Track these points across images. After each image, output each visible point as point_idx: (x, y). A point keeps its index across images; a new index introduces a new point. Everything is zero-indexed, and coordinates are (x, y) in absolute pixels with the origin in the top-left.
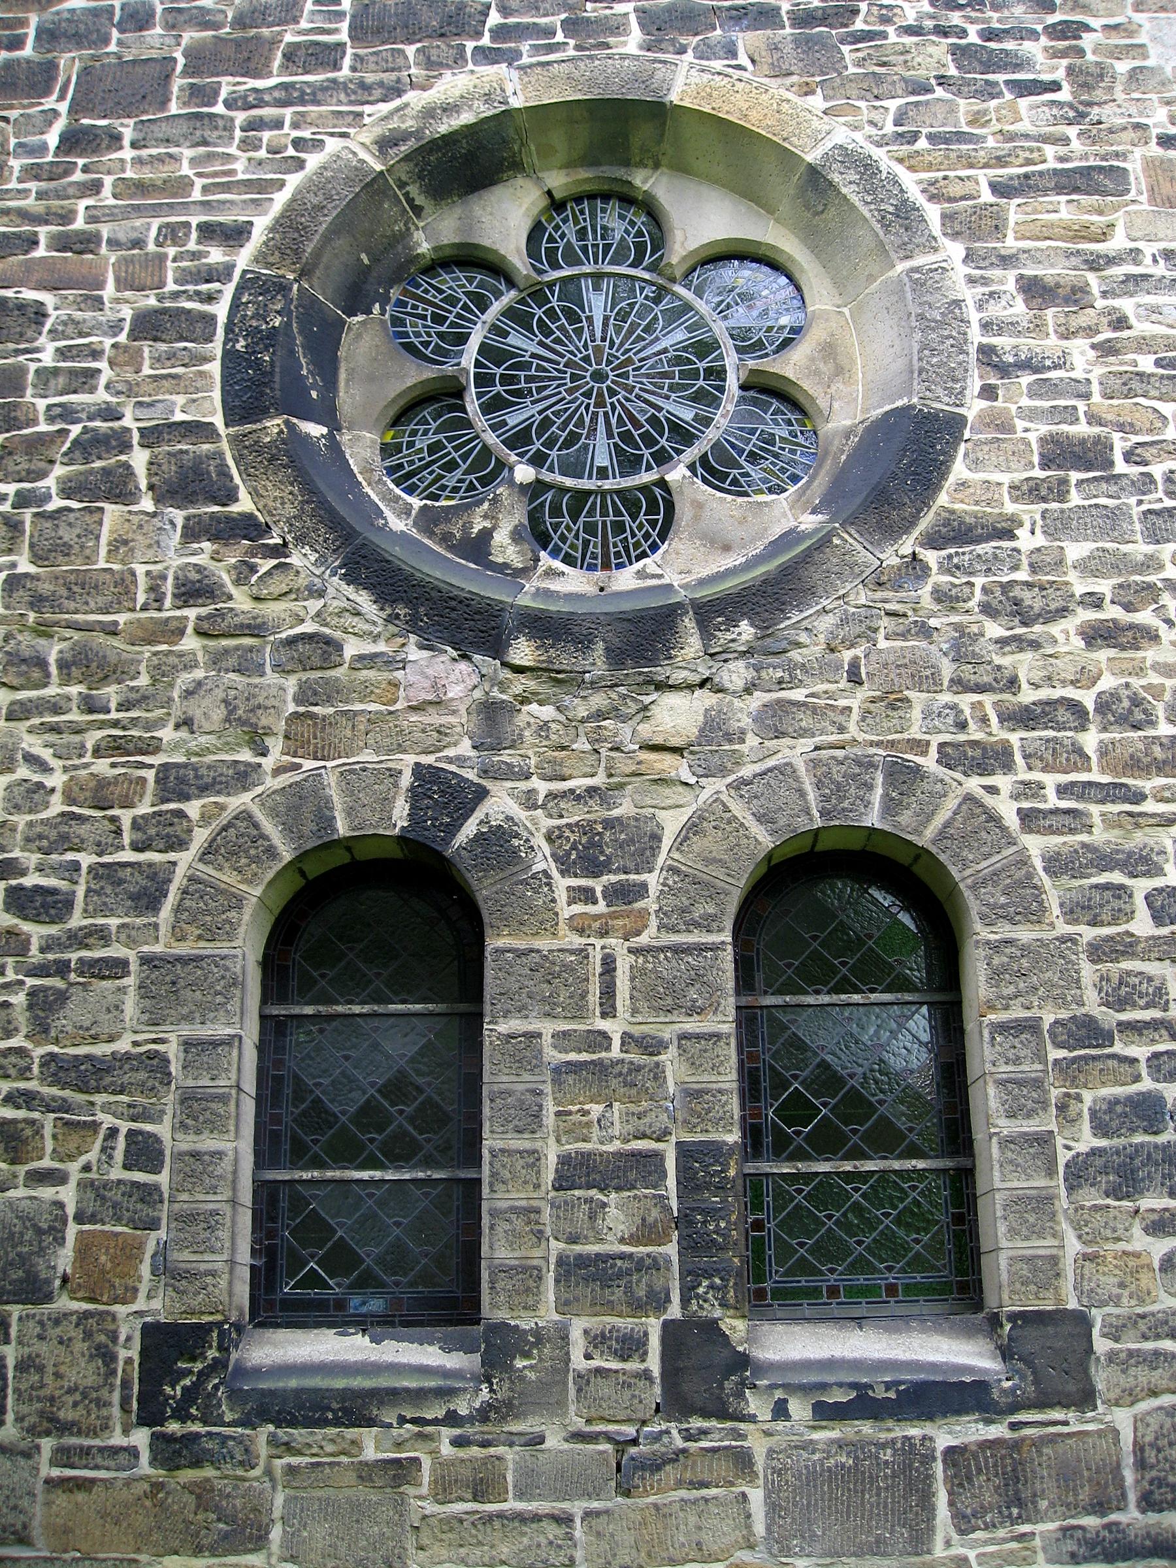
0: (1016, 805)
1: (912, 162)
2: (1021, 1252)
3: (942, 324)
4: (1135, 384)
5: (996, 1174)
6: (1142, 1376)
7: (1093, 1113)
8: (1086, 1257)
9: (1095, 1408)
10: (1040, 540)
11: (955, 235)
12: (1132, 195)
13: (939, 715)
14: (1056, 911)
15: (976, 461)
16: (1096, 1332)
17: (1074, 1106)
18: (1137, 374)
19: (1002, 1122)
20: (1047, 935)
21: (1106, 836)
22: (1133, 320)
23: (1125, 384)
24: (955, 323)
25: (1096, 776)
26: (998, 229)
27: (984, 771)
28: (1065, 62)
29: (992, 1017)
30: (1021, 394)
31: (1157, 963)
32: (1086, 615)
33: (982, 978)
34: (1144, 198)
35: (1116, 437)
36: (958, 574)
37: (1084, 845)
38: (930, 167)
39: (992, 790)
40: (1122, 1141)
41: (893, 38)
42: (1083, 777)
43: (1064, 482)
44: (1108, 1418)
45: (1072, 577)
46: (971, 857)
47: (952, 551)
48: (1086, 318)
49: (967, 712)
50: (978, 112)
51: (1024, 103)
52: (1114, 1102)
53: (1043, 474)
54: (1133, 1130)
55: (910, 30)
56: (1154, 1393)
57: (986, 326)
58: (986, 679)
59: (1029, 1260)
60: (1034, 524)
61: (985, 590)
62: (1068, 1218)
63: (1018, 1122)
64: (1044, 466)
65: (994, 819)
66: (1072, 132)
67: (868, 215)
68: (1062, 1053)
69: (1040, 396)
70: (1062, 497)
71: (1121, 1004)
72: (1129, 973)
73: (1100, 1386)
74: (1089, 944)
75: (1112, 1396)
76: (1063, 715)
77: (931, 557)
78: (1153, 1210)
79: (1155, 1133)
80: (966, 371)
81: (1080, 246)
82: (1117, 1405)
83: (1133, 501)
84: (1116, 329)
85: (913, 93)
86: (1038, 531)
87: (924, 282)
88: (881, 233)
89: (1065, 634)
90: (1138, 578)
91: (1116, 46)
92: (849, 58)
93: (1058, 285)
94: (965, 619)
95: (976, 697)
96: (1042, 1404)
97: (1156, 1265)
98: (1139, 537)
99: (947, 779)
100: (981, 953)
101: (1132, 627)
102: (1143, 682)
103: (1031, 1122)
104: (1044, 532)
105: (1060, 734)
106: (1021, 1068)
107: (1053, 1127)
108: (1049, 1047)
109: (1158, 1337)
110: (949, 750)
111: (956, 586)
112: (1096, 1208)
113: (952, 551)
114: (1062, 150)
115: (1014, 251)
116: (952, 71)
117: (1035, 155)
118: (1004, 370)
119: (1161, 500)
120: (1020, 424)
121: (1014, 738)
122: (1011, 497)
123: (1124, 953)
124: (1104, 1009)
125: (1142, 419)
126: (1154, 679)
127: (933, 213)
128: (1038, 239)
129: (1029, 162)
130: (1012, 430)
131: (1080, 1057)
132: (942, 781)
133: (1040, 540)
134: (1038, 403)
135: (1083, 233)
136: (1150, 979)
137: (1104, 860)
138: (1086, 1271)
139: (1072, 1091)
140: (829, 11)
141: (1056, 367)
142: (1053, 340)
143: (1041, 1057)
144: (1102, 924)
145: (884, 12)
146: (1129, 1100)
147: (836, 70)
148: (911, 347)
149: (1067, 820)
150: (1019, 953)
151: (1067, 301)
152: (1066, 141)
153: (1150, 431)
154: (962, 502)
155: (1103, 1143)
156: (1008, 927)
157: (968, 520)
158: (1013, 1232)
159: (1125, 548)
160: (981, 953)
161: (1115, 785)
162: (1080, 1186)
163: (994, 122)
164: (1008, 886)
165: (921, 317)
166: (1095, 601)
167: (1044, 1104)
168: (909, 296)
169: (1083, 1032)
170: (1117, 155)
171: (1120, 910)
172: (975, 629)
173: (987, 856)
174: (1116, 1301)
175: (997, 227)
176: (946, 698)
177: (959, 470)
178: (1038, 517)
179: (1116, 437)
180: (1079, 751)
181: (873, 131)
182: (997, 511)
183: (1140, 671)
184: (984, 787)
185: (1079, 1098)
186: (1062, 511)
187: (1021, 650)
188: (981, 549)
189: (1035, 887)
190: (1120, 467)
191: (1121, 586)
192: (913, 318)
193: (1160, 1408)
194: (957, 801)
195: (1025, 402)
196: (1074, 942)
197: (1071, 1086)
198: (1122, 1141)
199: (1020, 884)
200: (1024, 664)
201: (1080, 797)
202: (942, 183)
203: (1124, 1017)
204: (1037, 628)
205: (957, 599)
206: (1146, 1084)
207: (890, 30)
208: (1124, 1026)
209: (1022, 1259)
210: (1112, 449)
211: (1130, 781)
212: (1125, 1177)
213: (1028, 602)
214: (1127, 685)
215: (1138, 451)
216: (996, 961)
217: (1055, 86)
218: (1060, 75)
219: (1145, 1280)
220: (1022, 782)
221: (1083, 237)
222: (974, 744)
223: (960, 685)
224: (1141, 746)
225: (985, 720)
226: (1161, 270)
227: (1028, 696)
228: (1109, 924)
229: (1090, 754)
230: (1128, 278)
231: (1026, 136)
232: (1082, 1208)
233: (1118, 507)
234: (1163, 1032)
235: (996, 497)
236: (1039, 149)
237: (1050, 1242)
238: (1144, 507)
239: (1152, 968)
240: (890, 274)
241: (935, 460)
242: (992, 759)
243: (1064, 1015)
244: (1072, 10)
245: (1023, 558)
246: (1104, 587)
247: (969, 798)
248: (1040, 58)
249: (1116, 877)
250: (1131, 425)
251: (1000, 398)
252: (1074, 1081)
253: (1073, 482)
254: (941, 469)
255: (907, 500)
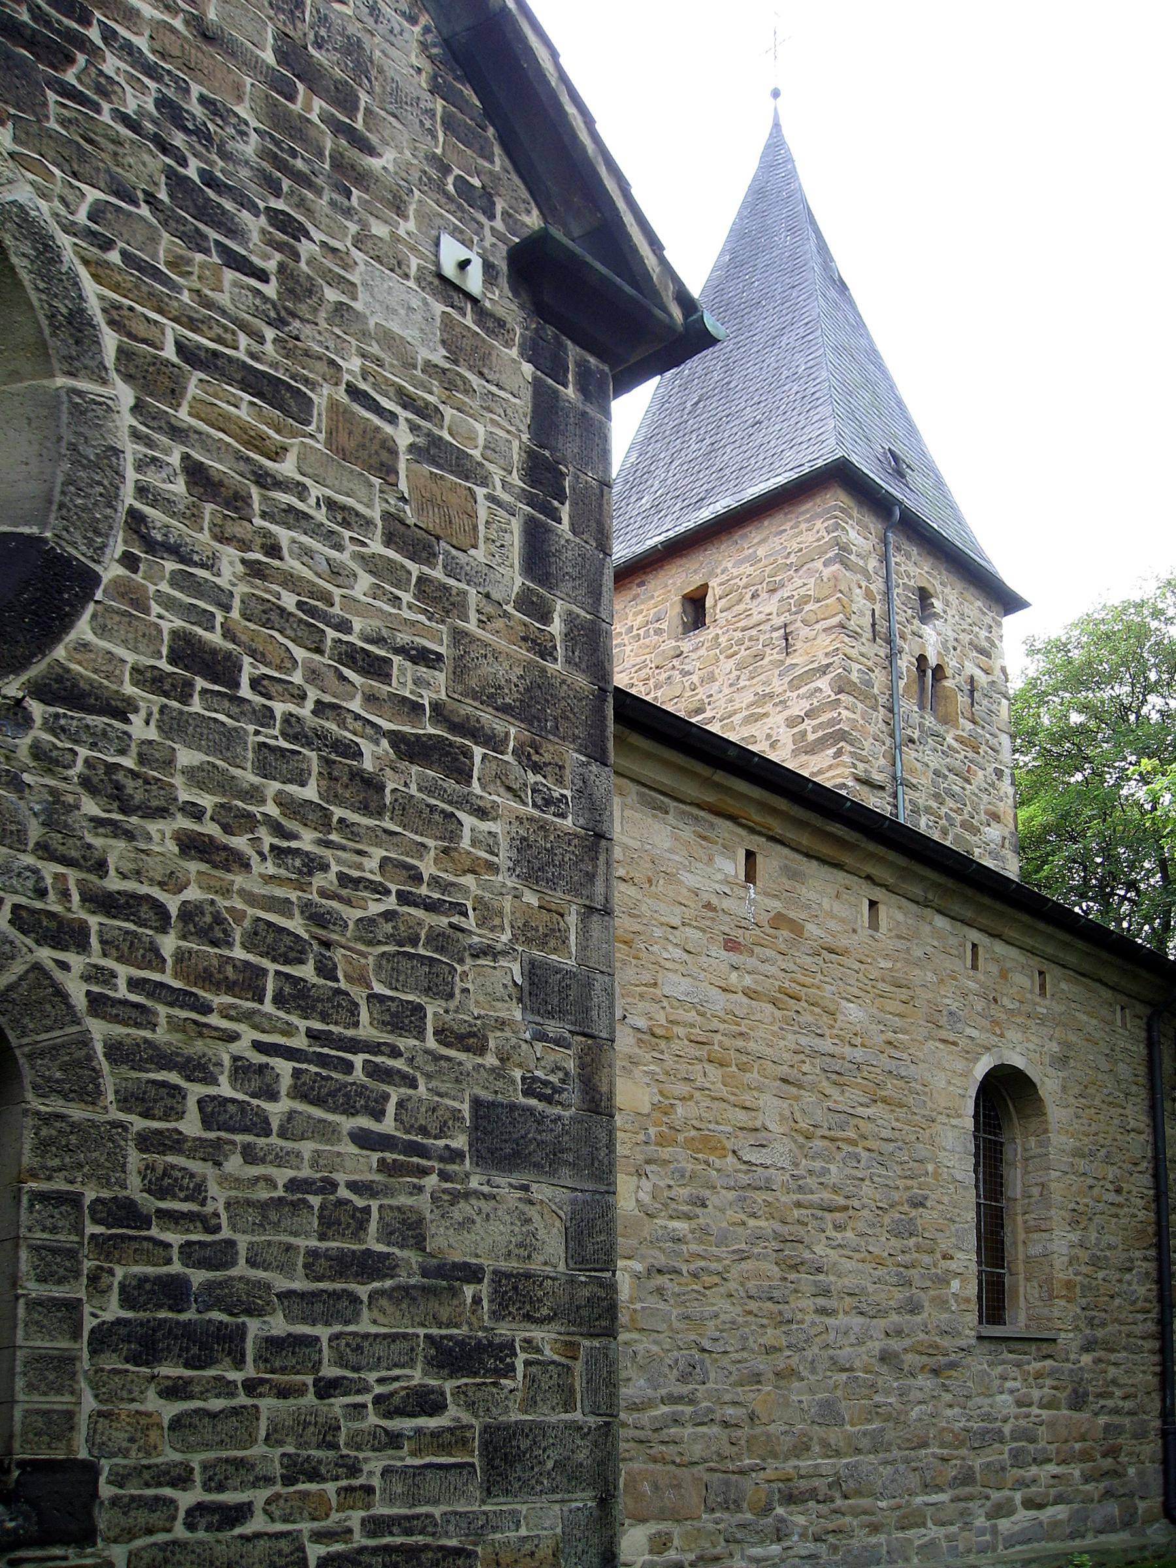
0: (85, 987)
1: (100, 271)
2: (37, 1406)
3: (95, 466)
4: (274, 616)
5: (20, 1333)
6: (142, 1517)
7: (122, 1286)
8: (100, 1414)
9: (94, 1544)
10: (152, 734)
11: (128, 378)
12: (310, 429)
13: (19, 875)
14: (111, 1097)
15: (104, 627)
16: (102, 1479)
17: (105, 1279)
18: (279, 607)
19: (31, 1285)
20: (100, 1118)
21: (168, 1038)
22: (285, 553)
23: (264, 612)
24: (109, 472)
25: (167, 979)
26: (175, 394)
27: (58, 945)
28: (278, 256)
29: (33, 1185)
30: (162, 578)
31: (200, 1163)
32: (184, 823)
33: (27, 1147)
34: (322, 437)
35: (247, 660)
36: (63, 737)
37: (146, 1041)
38: (116, 288)
39: (64, 966)
40: (147, 1315)
41: (106, 117)
42: (156, 977)
43: (190, 684)
44: (106, 1553)
45: (178, 781)
46: (31, 1026)
47: (61, 711)
48: (239, 529)
49: (49, 881)
50: (181, 257)
51: (229, 275)
52: (143, 1280)
53: (170, 669)
54: (159, 1307)
55: (125, 119)
56: (150, 1532)
57: (142, 491)
58: (74, 854)
59: (46, 1413)
60: (150, 715)
61: (87, 761)
62: (86, 1378)
63: (48, 1287)
64: (172, 661)
65: (61, 994)
66: (270, 334)
67: (36, 303)
68: (99, 1229)
69: (181, 589)
70: (185, 699)
71: (161, 1193)
72: (173, 1167)
73: (102, 1526)
74: (138, 1134)
75: (111, 1534)
76: (145, 912)
77: (37, 709)
78: (168, 1377)
79: (179, 1311)
80: (111, 528)
81: (251, 454)
82: (116, 1541)
83: (251, 728)
84: (267, 554)
85: (116, 194)
86: (153, 723)
87: (88, 413)
88: (47, 331)
89: (161, 834)
90: (240, 804)
91: (330, 271)
92: (52, 108)
93: (221, 484)
94: (62, 785)
95: (61, 869)
96: (42, 1543)
97: (166, 1424)
98: (249, 765)
99: (17, 942)
100: (29, 1122)
101: (226, 848)
102: (227, 903)
103: (61, 1288)
104: (159, 727)
105: (140, 930)
106: (57, 1237)
107: (82, 1295)
108: (87, 1221)
109: (159, 1485)
110: (24, 914)
111: (57, 748)
112: (115, 1372)
113: (61, 711)
114: (256, 348)
115: (185, 425)
116: (163, 195)
117: (228, 336)
118: (151, 546)
119: (276, 738)
120: (156, 609)
121: (94, 921)
122: (132, 679)
123: (171, 1148)
124: (145, 1195)
125: (274, 655)
126: (239, 905)
127: (110, 340)
128: (212, 426)
129: (219, 340)
130: (146, 610)
131: (116, 1235)
132: (12, 942)
133: (152, 734)
134: (177, 594)
135: (256, 442)
136: (192, 1176)
137: (165, 1060)
138: (99, 1426)
139: (106, 1265)
140: (39, 38)
141: (203, 566)
142: (205, 537)
143: (78, 1229)
144: (153, 1118)
145: (102, 80)
146: (158, 1279)
147: (35, 114)
148: (54, 474)
149: (134, 1014)
150: (68, 1129)
151: (227, 504)
152: (261, 340)
153: (279, 668)
154: (80, 664)
155: (129, 1315)
156: (61, 1102)
157: (82, 684)
158: (31, 1387)
159: (237, 772)
160: (29, 1122)
161: (186, 993)
162: (102, 1351)
163: (195, 277)
164: (65, 1063)
165: (73, 447)
166: (195, 812)
167: (77, 1274)
168: (65, 418)
169: (122, 1213)
170: (306, 381)
171: (172, 1108)
172: (70, 799)
173: (48, 1030)
174: (125, 1453)
175: (173, 391)
176: (29, 860)
177: (83, 629)
178: (155, 710)
179: (247, 660)
180: (155, 950)
181: (63, 211)
182: (114, 687)
183: (226, 892)
184: (56, 961)
185: (111, 1272)
186: (181, 713)
187: (115, 836)
188: (92, 720)
189: (94, 1069)
190: (245, 691)
191: (222, 806)
192: (64, 444)
193: (155, 1544)
194: (24, 967)
195: (164, 587)
196: (126, 1129)
197: (105, 1261)
198: (147, 1315)
199: (78, 1063)
200: (116, 851)
201: (150, 995)
202: (126, 313)
203: (163, 1205)
204: (134, 820)
205: (57, 763)
206: (176, 1268)
207: (106, 107)
208: (162, 1214)
209: (38, 1412)
210: (240, 671)
211: (201, 993)
212: (146, 1345)
213: (129, 791)
214: (212, 902)
215: (265, 682)
216: (44, 1132)
217: (263, 276)
218: (271, 266)
219: (154, 1435)
220: (95, 966)
221: (256, 447)
222: (52, 915)
223: (45, 850)
224: (215, 962)
225: (65, 894)
226: (321, 515)
227: (113, 883)
228: (160, 1119)
229: (166, 956)
230: (290, 509)
231: (224, 313)
232: (102, 1370)
233: (236, 729)
234: (199, 1224)
235: (117, 672)
236: (234, 333)
237: (68, 1398)
238: (261, 739)
239: (195, 1166)
240: (46, 382)
241: (59, 608)
242: (71, 936)
243: (106, 1194)
244: (298, 206)
245: (133, 745)
246: (207, 801)
247: (37, 967)
248: (255, 237)
249: (173, 1078)
250: (263, 655)
251: (140, 574)
252: (108, 1257)
253: (198, 688)
254: (67, 622)
255: (20, 638)
